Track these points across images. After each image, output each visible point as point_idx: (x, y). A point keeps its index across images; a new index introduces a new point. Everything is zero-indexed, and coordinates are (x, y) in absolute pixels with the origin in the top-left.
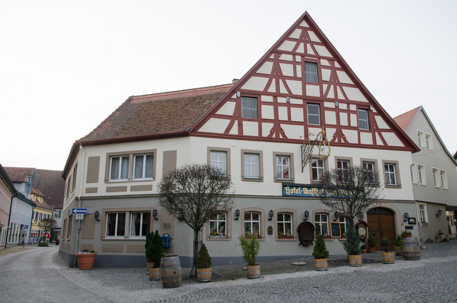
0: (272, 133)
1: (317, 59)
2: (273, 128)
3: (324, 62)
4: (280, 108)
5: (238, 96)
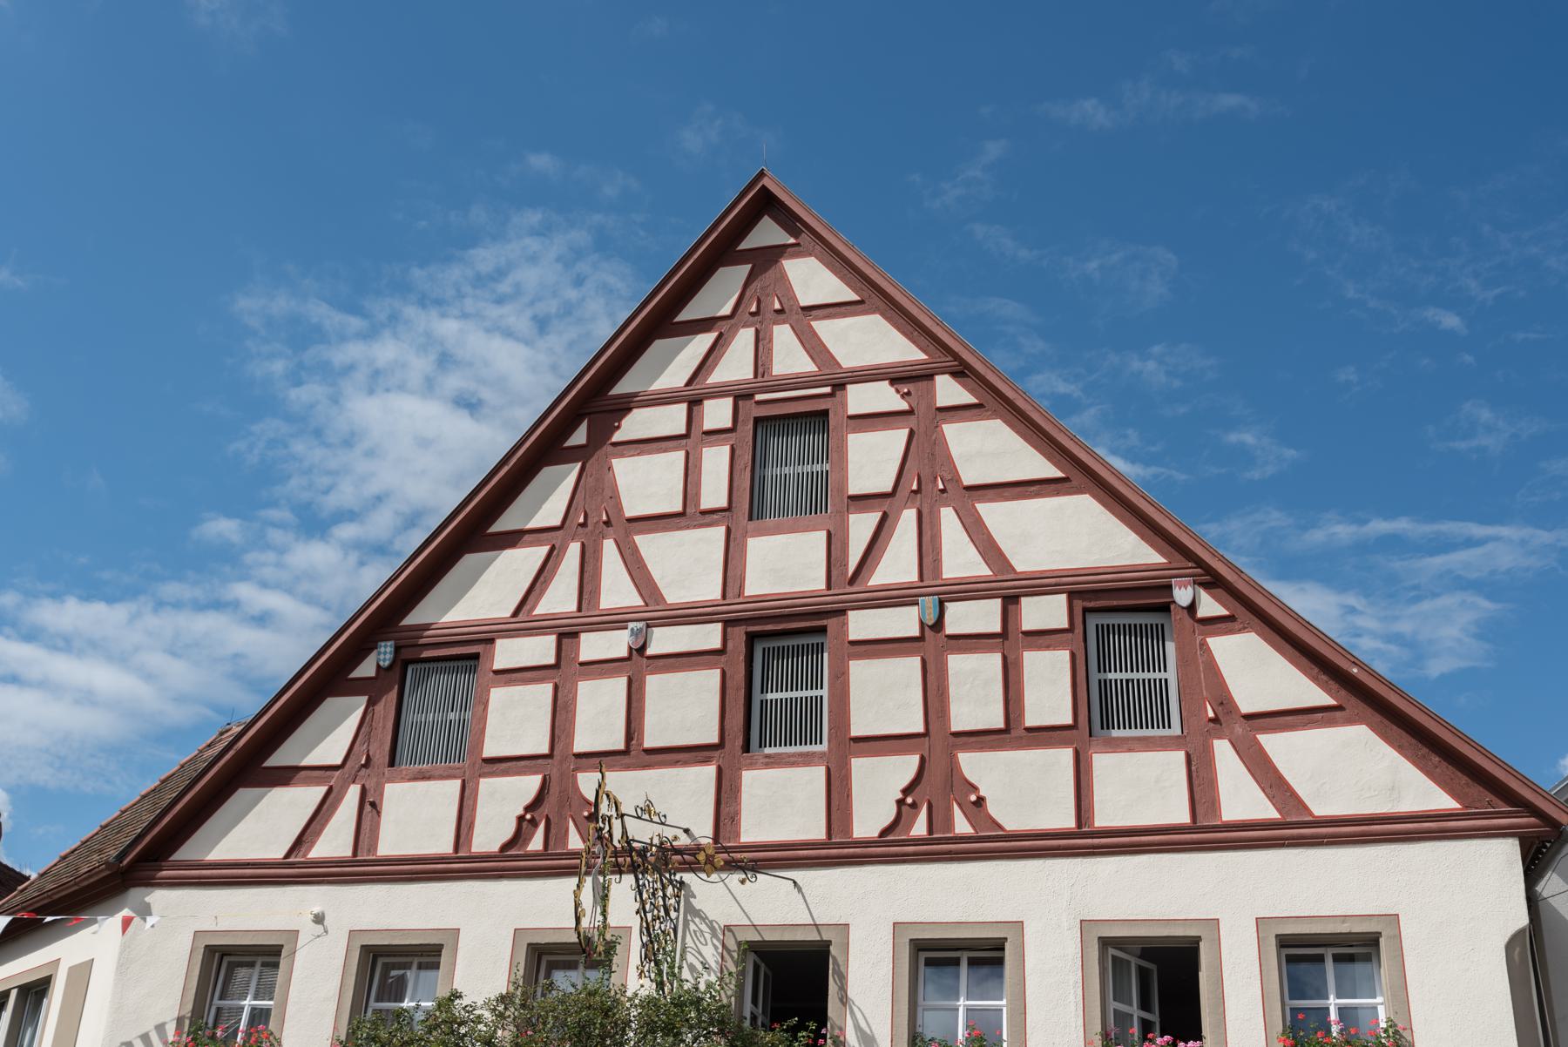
1: (827, 390)
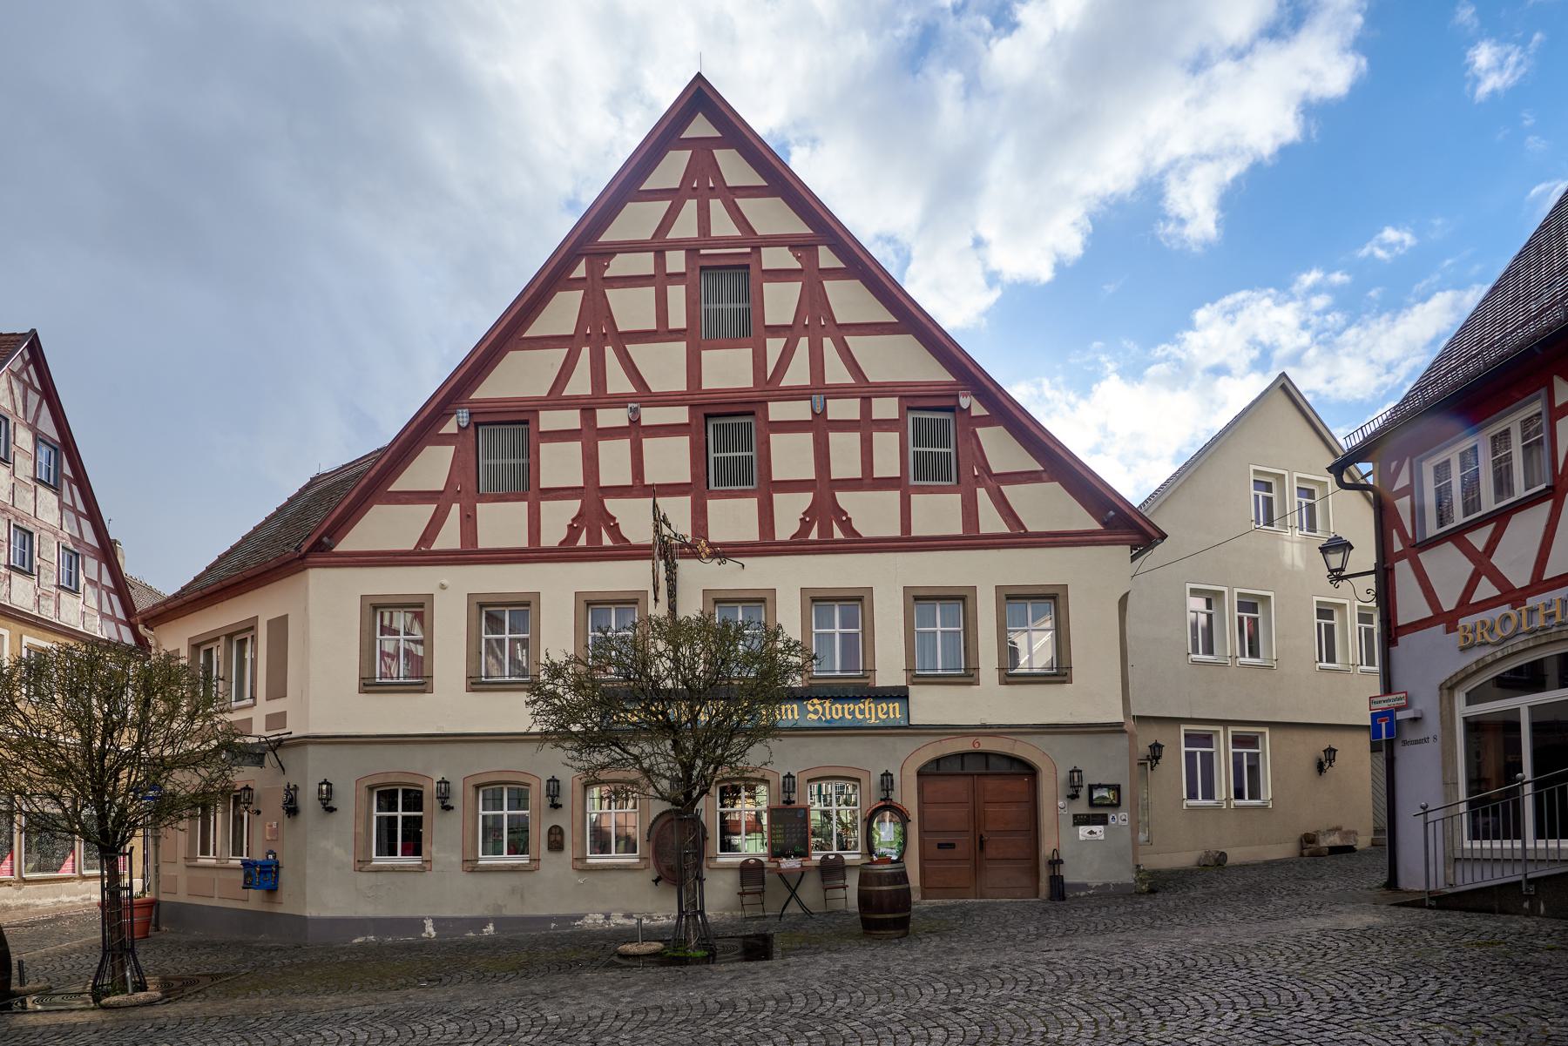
1: (748, 250)
2: (579, 515)
4: (835, 438)
5: (461, 424)
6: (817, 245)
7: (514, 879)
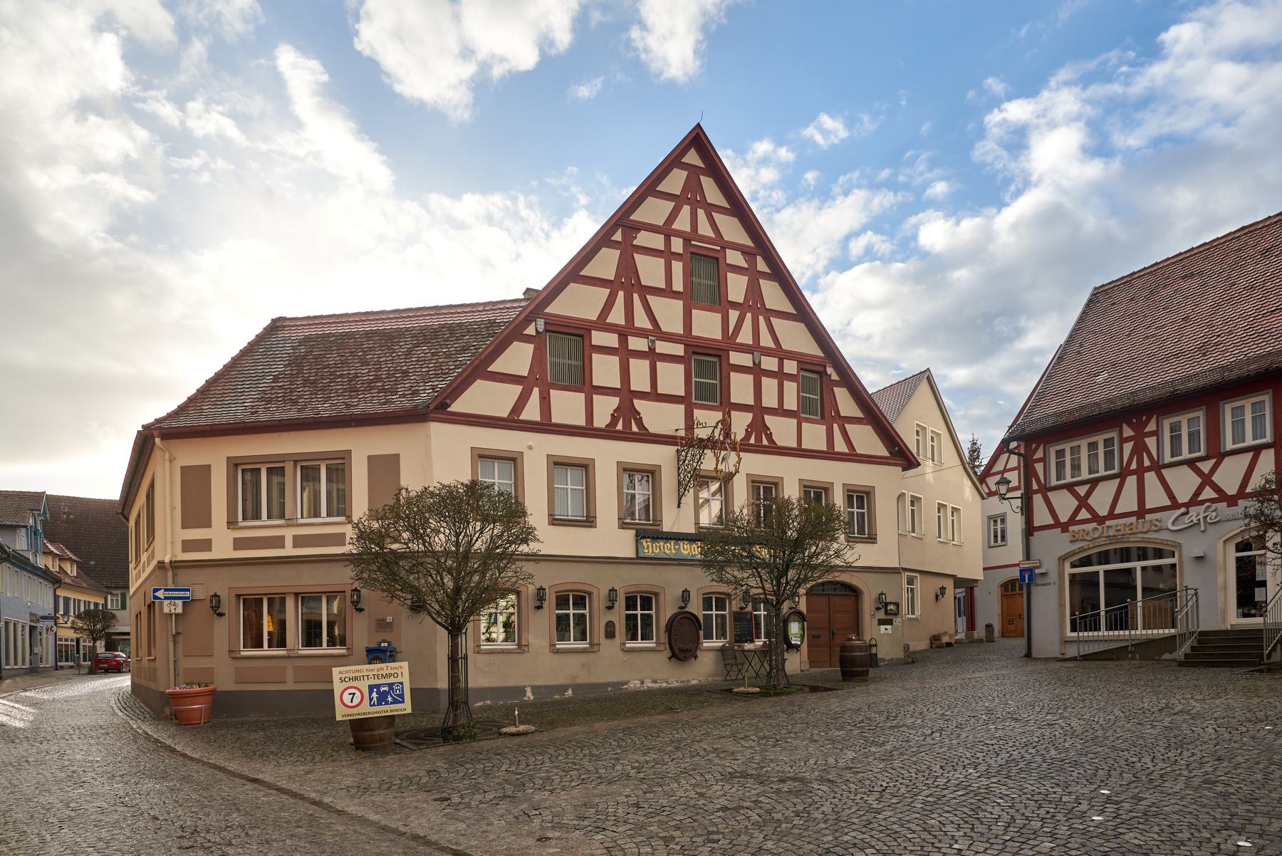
0: (614, 419)
1: (719, 248)
2: (618, 408)
3: (734, 258)
4: (633, 362)
5: (539, 330)
6: (756, 255)
7: (583, 658)
